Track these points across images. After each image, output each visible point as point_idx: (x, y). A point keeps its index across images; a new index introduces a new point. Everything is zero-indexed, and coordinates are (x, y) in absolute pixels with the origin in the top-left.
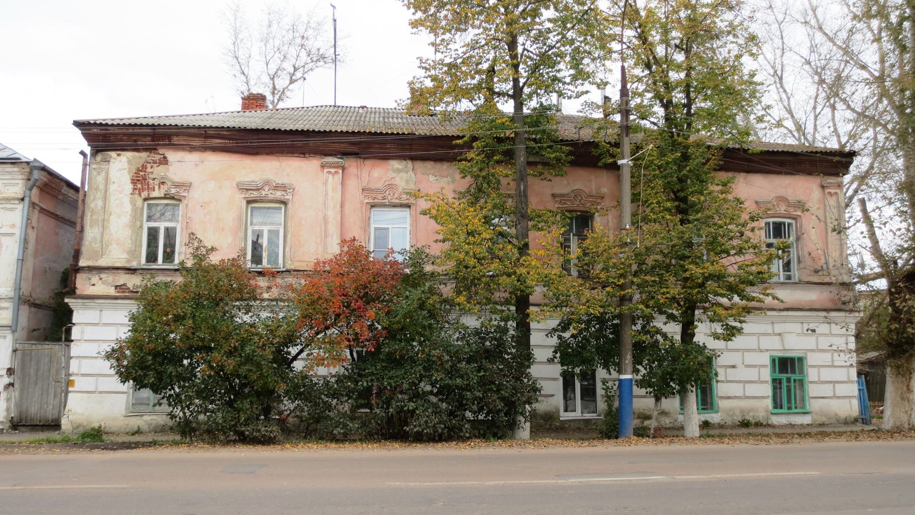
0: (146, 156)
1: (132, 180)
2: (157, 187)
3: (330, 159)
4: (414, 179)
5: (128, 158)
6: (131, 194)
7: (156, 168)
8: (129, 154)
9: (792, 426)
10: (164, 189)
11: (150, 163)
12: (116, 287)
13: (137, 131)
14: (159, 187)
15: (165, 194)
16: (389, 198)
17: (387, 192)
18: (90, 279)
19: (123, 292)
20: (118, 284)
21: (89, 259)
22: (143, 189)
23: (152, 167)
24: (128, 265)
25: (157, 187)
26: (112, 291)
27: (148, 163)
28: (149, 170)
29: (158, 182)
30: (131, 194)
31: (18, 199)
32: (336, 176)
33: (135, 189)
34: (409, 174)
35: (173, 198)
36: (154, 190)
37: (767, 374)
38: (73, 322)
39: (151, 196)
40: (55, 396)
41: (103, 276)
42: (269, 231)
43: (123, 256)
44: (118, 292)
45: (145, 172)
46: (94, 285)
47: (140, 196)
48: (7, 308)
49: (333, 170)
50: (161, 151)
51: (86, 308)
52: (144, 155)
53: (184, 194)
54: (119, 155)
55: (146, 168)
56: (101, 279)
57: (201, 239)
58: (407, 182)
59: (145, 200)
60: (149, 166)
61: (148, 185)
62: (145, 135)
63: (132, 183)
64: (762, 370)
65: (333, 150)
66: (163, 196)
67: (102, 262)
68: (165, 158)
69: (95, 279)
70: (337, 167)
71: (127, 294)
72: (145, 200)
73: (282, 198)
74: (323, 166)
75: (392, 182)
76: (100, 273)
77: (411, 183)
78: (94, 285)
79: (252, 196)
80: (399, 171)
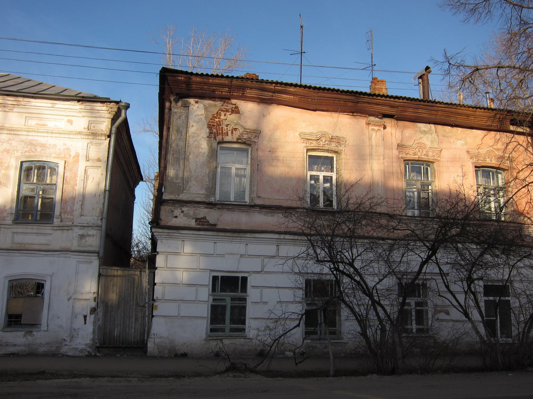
0: (220, 105)
1: (208, 124)
2: (230, 133)
3: (372, 118)
4: (437, 140)
5: (205, 106)
6: (208, 137)
7: (229, 116)
8: (207, 102)
9: (146, 327)
10: (236, 134)
11: (223, 111)
12: (197, 220)
13: (217, 81)
14: (232, 133)
15: (238, 139)
16: (419, 154)
17: (417, 150)
18: (172, 211)
19: (202, 225)
20: (198, 217)
21: (171, 193)
22: (217, 133)
23: (225, 115)
24: (207, 201)
25: (230, 133)
26: (193, 223)
27: (222, 111)
28: (222, 117)
29: (231, 128)
30: (208, 137)
31: (105, 135)
32: (378, 133)
33: (211, 133)
34: (433, 135)
35: (244, 143)
36: (228, 135)
37: (205, 294)
38: (158, 250)
39: (225, 140)
40: (136, 319)
41: (185, 209)
42: (324, 177)
43: (202, 192)
44: (198, 224)
45: (219, 118)
46: (176, 217)
47: (216, 139)
48: (93, 236)
49: (376, 128)
50: (234, 101)
51: (170, 237)
52: (219, 103)
53: (255, 140)
54: (197, 102)
55: (220, 116)
56: (182, 212)
57: (14, 174)
58: (432, 142)
59: (219, 143)
60: (223, 114)
61: (222, 130)
62: (223, 86)
63: (208, 127)
64: (201, 289)
65: (376, 112)
66: (235, 140)
67: (183, 197)
68: (237, 107)
69: (177, 212)
70: (380, 126)
71: (206, 227)
72: (219, 143)
73: (336, 149)
74: (368, 124)
75: (420, 141)
76: (183, 206)
77: (435, 143)
78: (176, 217)
79: (312, 145)
80: (425, 132)
